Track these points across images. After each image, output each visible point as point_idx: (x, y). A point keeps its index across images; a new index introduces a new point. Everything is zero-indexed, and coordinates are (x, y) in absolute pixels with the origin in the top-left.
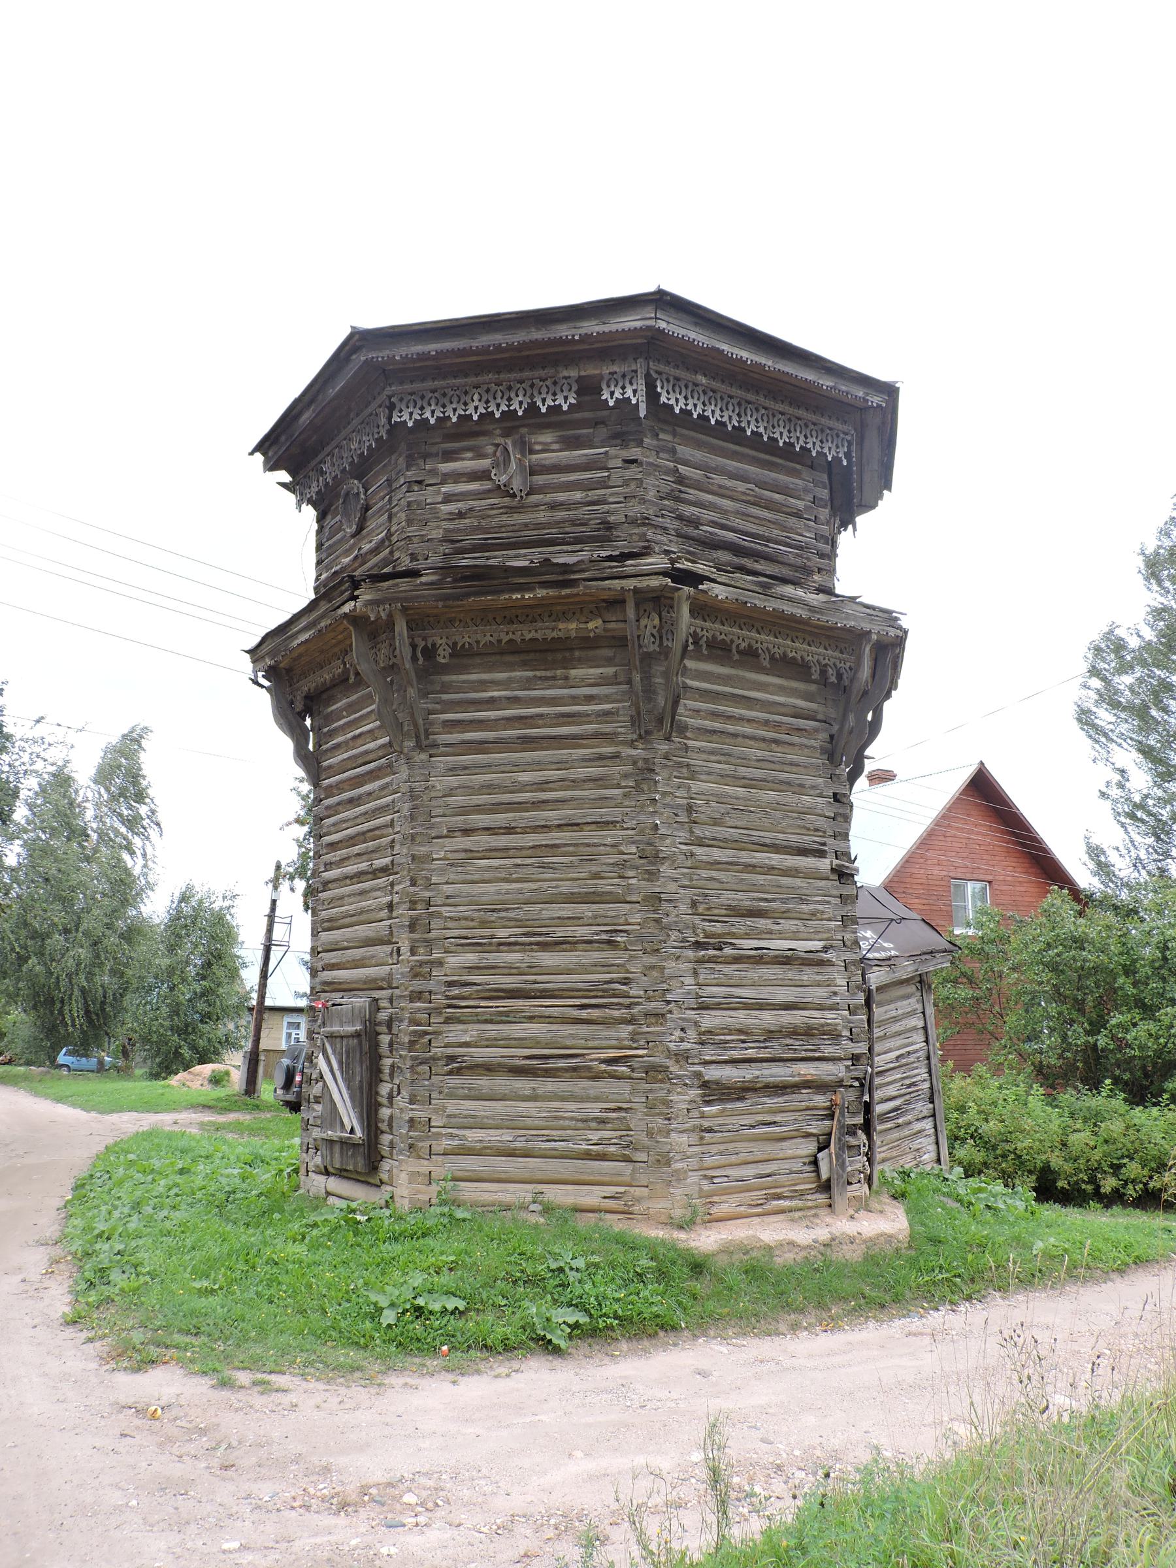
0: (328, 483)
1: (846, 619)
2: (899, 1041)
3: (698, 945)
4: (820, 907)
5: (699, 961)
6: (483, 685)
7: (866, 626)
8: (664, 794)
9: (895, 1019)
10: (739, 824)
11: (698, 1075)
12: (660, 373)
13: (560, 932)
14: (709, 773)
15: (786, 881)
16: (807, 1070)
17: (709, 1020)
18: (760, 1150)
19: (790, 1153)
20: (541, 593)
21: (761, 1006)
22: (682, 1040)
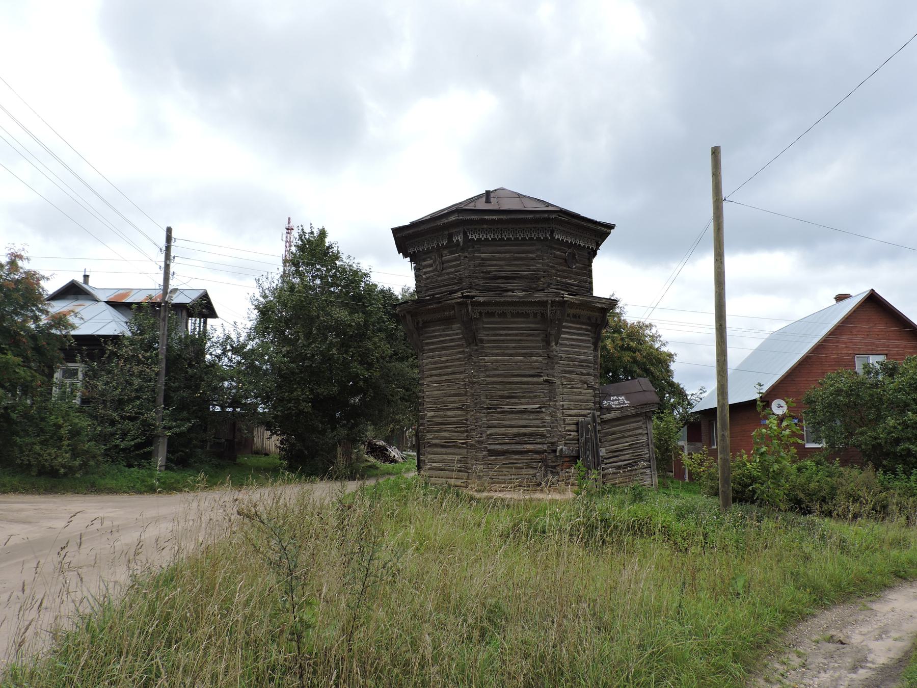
0: (244, 348)
2: (632, 439)
3: (487, 408)
5: (488, 413)
6: (434, 331)
7: (545, 299)
8: (475, 363)
9: (629, 430)
11: (486, 447)
12: (468, 229)
13: (452, 405)
15: (526, 386)
17: (490, 431)
20: (435, 306)
22: (481, 437)
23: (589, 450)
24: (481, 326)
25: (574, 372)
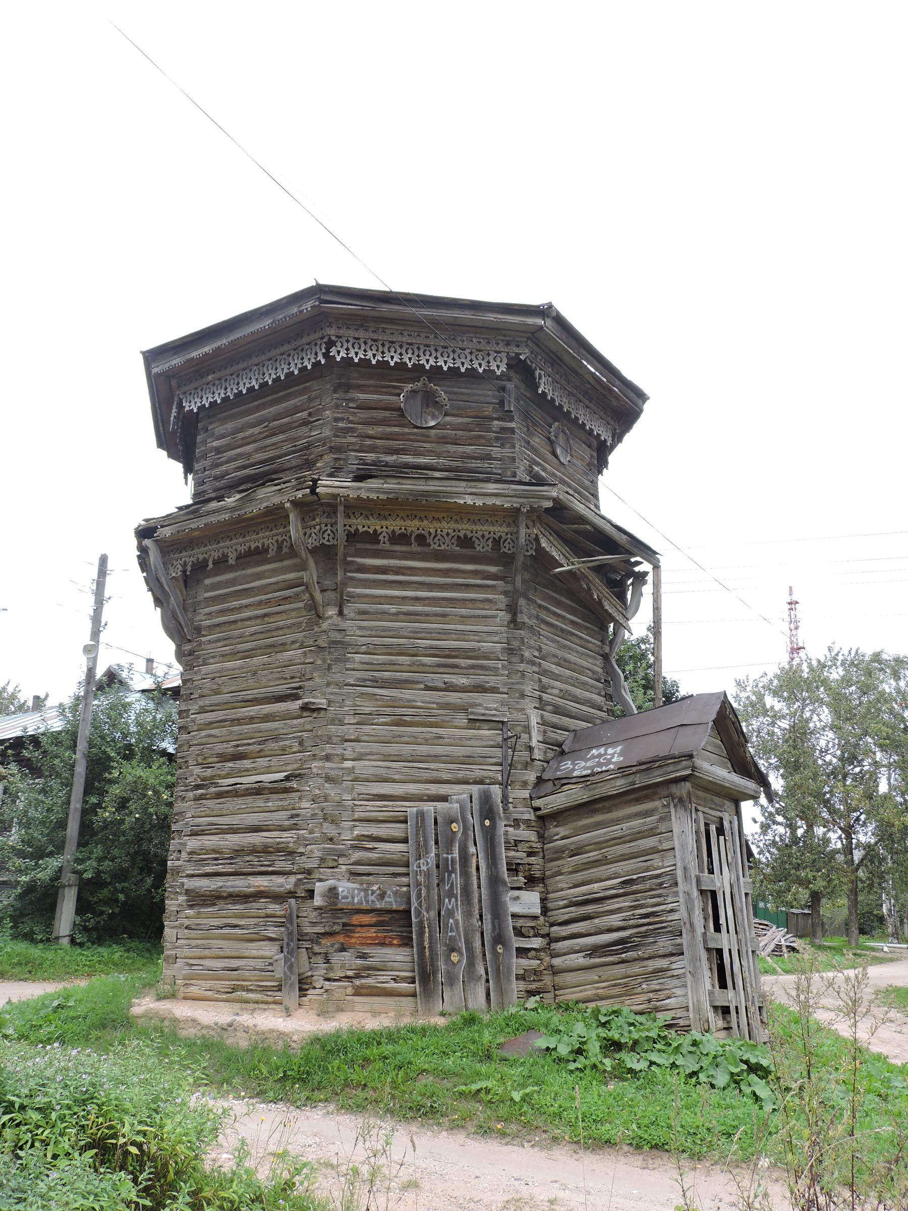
1: (260, 503)
4: (287, 743)
7: (276, 500)
10: (233, 689)
14: (213, 657)
15: (264, 726)
16: (261, 883)
18: (229, 947)
19: (255, 953)
21: (234, 830)
23: (451, 894)
24: (200, 598)
25: (418, 682)
